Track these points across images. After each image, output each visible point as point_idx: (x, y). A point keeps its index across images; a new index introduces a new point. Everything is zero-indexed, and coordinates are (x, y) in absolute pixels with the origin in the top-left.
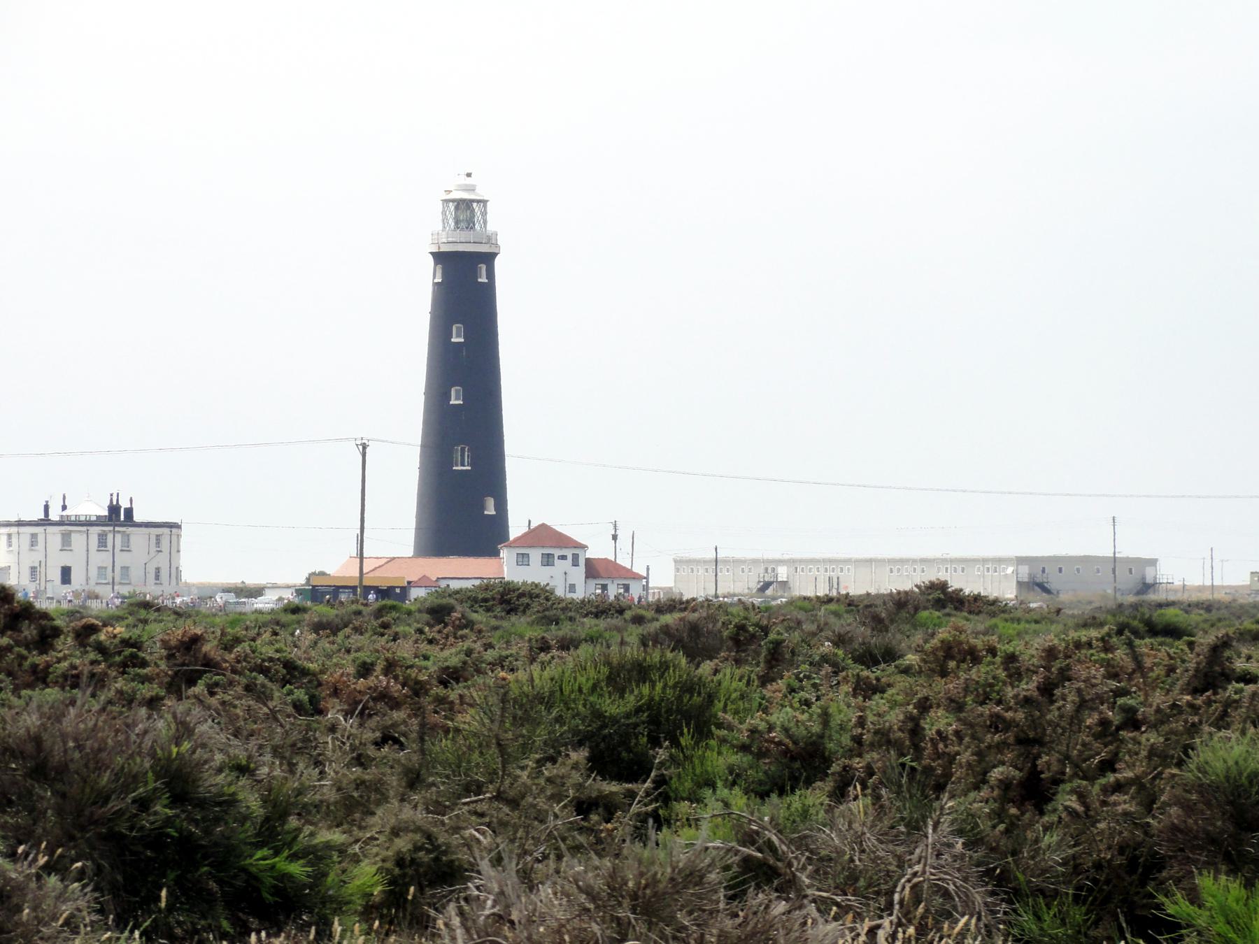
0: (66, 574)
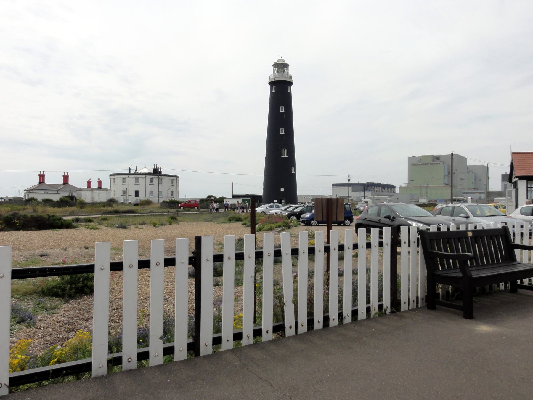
0: (137, 193)
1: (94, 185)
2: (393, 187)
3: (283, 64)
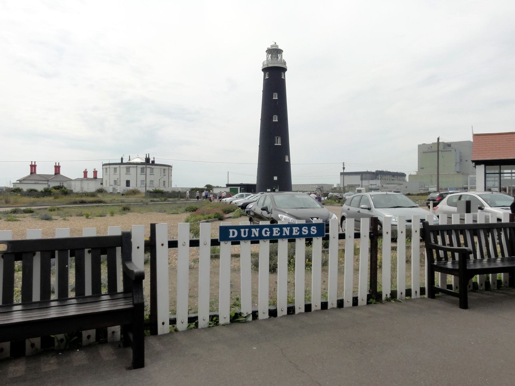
0: (128, 183)
1: (90, 175)
2: (403, 175)
3: (276, 49)
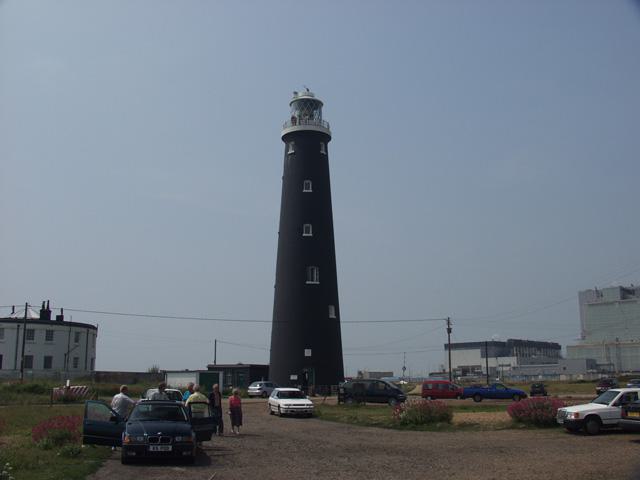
2: (557, 347)
